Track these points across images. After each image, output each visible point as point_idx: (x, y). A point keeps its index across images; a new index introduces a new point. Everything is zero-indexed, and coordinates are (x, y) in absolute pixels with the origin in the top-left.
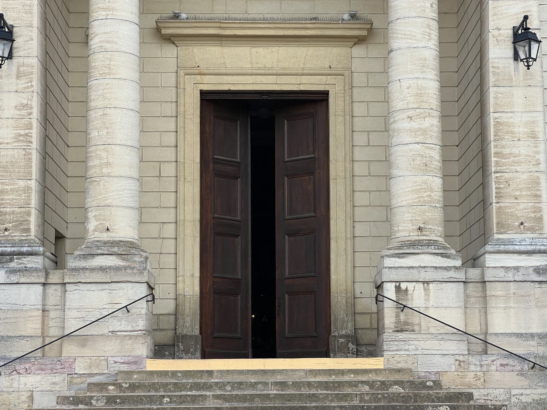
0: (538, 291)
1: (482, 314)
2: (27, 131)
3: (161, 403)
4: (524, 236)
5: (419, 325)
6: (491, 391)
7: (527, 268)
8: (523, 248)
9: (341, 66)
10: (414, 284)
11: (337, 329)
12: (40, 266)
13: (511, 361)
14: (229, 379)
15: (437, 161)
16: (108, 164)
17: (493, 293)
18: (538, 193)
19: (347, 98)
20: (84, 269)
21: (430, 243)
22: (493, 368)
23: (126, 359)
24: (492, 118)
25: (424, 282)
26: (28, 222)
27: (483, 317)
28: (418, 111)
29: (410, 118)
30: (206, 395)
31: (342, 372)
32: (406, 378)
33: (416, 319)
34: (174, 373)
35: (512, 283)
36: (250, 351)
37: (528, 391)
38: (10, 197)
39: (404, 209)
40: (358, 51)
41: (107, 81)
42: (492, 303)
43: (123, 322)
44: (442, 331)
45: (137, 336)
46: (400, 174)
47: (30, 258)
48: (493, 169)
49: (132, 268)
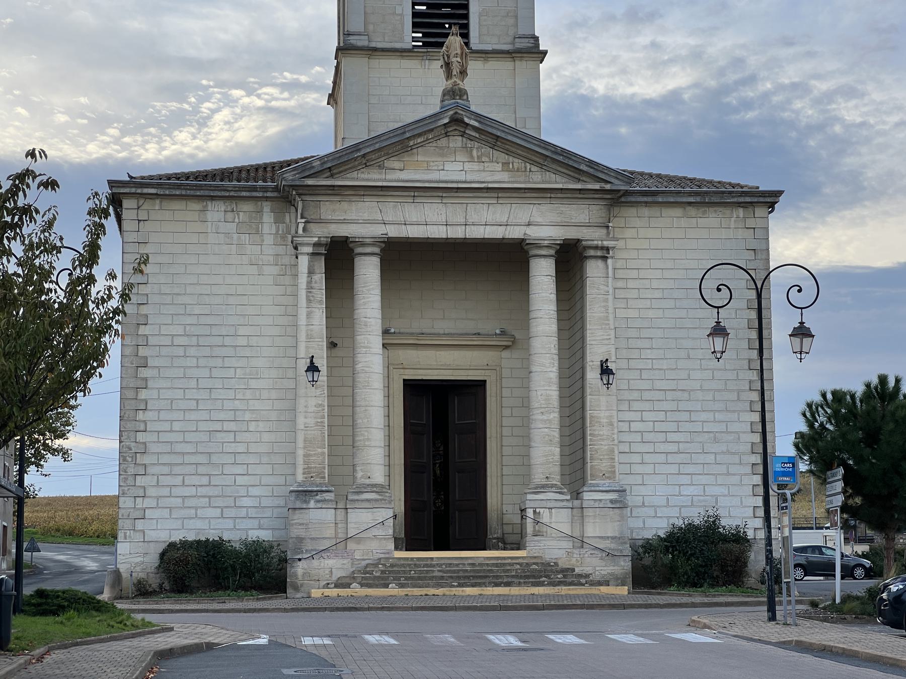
0: (612, 513)
1: (581, 526)
2: (322, 420)
3: (410, 574)
4: (605, 481)
5: (546, 532)
6: (584, 568)
7: (606, 500)
8: (604, 489)
9: (495, 364)
11: (491, 534)
12: (333, 498)
13: (596, 552)
14: (442, 562)
16: (368, 439)
17: (588, 514)
18: (613, 457)
19: (498, 385)
20: (357, 500)
21: (552, 486)
22: (586, 555)
23: (384, 551)
24: (588, 413)
25: (549, 508)
26: (324, 473)
27: (581, 528)
29: (542, 413)
30: (362, 585)
31: (504, 558)
32: (539, 561)
33: (545, 529)
34: (412, 559)
36: (432, 547)
37: (605, 568)
38: (314, 458)
39: (538, 466)
40: (505, 354)
41: (366, 390)
42: (586, 520)
43: (380, 530)
44: (558, 536)
45: (389, 538)
46: (536, 445)
47: (327, 494)
48: (589, 443)
49: (385, 500)
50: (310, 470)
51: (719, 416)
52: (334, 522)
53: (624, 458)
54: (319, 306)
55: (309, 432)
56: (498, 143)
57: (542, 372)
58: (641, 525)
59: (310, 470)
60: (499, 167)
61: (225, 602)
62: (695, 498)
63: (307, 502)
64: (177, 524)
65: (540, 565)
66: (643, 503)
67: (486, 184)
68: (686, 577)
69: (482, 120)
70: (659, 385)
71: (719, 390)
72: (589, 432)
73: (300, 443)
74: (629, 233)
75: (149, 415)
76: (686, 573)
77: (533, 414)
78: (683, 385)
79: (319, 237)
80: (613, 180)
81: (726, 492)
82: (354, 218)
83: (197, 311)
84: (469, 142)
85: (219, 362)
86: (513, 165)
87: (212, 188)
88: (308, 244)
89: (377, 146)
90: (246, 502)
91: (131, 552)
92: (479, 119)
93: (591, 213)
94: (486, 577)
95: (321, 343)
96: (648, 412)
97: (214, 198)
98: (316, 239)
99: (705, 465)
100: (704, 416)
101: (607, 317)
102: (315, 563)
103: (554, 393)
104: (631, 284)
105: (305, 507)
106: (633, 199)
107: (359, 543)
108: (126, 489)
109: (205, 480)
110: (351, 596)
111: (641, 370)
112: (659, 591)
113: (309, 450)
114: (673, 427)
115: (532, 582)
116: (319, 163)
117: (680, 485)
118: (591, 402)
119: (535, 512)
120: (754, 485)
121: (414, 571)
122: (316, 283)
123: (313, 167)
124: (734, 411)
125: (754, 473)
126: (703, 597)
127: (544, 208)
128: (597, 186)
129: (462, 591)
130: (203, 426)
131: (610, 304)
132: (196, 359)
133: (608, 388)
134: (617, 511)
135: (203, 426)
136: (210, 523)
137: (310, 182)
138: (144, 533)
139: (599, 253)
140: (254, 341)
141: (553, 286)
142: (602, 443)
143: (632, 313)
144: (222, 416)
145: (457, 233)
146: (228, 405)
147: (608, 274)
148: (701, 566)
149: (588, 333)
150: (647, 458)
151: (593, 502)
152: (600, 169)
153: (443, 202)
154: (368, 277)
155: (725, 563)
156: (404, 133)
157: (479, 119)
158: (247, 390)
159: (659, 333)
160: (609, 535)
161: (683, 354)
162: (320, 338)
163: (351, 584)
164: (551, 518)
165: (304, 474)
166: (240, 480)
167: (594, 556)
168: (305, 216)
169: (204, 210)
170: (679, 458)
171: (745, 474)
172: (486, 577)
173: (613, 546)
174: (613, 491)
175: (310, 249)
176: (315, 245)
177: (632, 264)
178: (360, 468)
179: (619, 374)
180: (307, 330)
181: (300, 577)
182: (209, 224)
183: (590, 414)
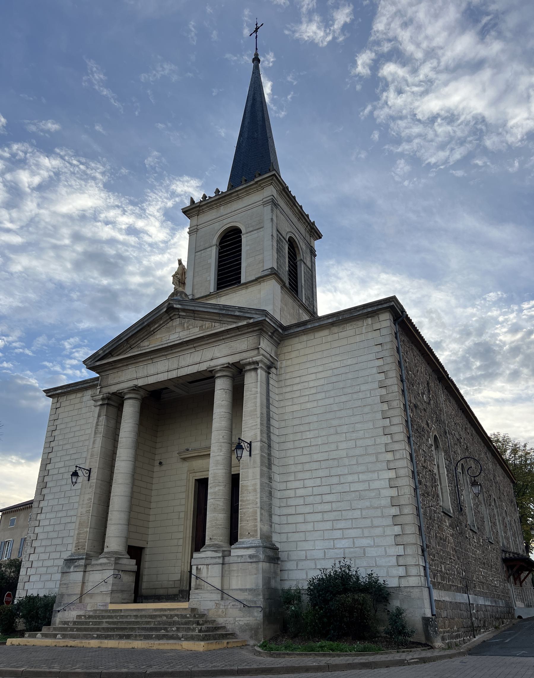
4: (250, 539)
5: (204, 586)
10: (203, 566)
15: (221, 506)
18: (256, 518)
22: (229, 607)
25: (207, 565)
28: (213, 484)
35: (240, 564)
37: (242, 619)
51: (362, 477)
55: (82, 518)
56: (196, 315)
60: (197, 329)
62: (347, 550)
65: (180, 616)
66: (306, 557)
69: (182, 303)
70: (316, 457)
74: (294, 354)
78: (334, 455)
80: (254, 316)
81: (372, 543)
87: (82, 383)
89: (130, 334)
92: (180, 303)
96: (309, 480)
100: (350, 478)
101: (256, 409)
107: (91, 598)
113: (80, 530)
114: (326, 489)
116: (102, 352)
117: (334, 540)
119: (197, 568)
123: (100, 355)
124: (374, 471)
128: (245, 323)
134: (254, 565)
139: (253, 367)
143: (296, 408)
145: (173, 375)
150: (309, 518)
151: (236, 557)
157: (180, 303)
159: (315, 418)
161: (332, 431)
164: (207, 573)
165: (75, 547)
167: (236, 607)
170: (332, 516)
171: (388, 526)
173: (250, 597)
174: (252, 547)
176: (103, 399)
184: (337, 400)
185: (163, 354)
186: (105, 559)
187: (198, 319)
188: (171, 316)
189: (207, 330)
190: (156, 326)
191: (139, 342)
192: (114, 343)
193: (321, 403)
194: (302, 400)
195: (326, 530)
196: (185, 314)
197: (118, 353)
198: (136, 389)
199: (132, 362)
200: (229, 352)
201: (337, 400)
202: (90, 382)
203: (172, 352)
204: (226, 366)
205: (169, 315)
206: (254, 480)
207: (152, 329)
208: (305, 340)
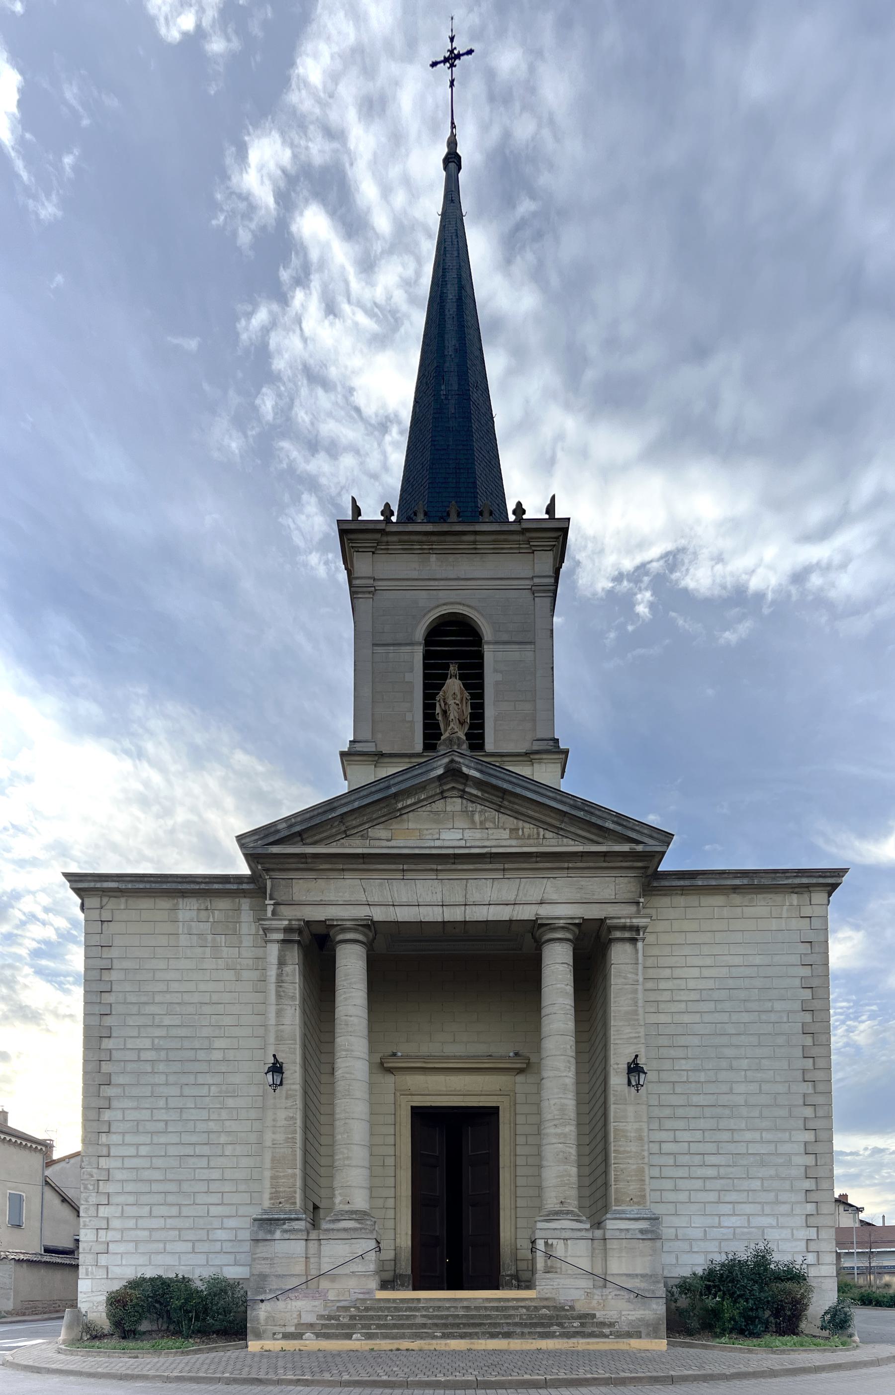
3: (386, 1320)
4: (633, 1208)
5: (561, 1268)
6: (607, 1312)
7: (634, 1230)
8: (632, 1216)
13: (622, 1293)
14: (432, 1304)
16: (348, 1158)
17: (611, 1247)
20: (333, 1230)
21: (568, 1212)
22: (610, 1297)
23: (362, 1291)
24: (612, 1126)
25: (564, 1239)
26: (295, 1198)
30: (318, 1335)
31: (508, 1300)
33: (558, 1264)
34: (394, 1300)
36: (445, 1285)
40: (520, 1078)
45: (369, 1275)
47: (297, 1222)
48: (613, 1162)
49: (365, 1229)
50: (278, 1195)
51: (767, 1136)
52: (304, 1255)
53: (656, 1184)
54: (291, 1003)
55: (277, 1150)
57: (556, 1077)
58: (674, 1261)
59: (278, 1195)
60: (506, 834)
61: (137, 1357)
62: (738, 1231)
63: (272, 1232)
64: (142, 1260)
66: (676, 1235)
67: (489, 849)
68: (732, 1322)
69: (484, 769)
70: (695, 1099)
71: (767, 1106)
72: (612, 1148)
73: (268, 1164)
75: (115, 1138)
76: (732, 1319)
77: (545, 1128)
78: (723, 1100)
79: (290, 920)
80: (646, 840)
81: (774, 1223)
82: (332, 898)
83: (167, 1022)
84: (470, 804)
85: (191, 1079)
86: (523, 831)
87: (179, 880)
88: (277, 930)
89: (356, 805)
90: (221, 1235)
91: (94, 1290)
92: (480, 767)
93: (617, 887)
94: (480, 1325)
95: (292, 1046)
97: (185, 895)
98: (286, 922)
99: (750, 1193)
100: (748, 1136)
101: (637, 1011)
102: (281, 1305)
103: (570, 1102)
104: (663, 985)
105: (269, 1238)
106: (667, 883)
108: (87, 1220)
109: (174, 1211)
110: (300, 1350)
111: (674, 1083)
112: (704, 1342)
113: (277, 1171)
114: (712, 1148)
115: (539, 1332)
116: (284, 825)
117: (719, 1216)
118: (615, 1112)
119: (546, 1243)
120: (807, 1215)
121: (391, 1316)
122: (287, 975)
123: (278, 831)
124: (785, 1130)
125: (808, 1200)
126: (767, 1354)
127: (560, 882)
128: (626, 848)
129: (446, 1344)
130: (172, 1150)
131: (640, 995)
132: (165, 1076)
133: (638, 1090)
134: (648, 1243)
135: (172, 1150)
136: (179, 1258)
137: (275, 849)
138: (107, 1268)
139: (627, 935)
140: (231, 1055)
141: (570, 977)
142: (630, 1161)
143: (663, 1018)
144: (194, 1139)
145: (455, 915)
146: (201, 1126)
147: (637, 959)
148: (752, 1309)
149: (613, 1032)
150: (682, 1184)
152: (630, 825)
153: (439, 877)
154: (349, 969)
155: (782, 1306)
156: (388, 787)
157: (480, 767)
158: (222, 1110)
159: (696, 1041)
160: (639, 1271)
161: (724, 1064)
162: (292, 1040)
163: (303, 1334)
164: (566, 1251)
165: (271, 1199)
166: (214, 1210)
168: (275, 896)
169: (175, 909)
170: (718, 1185)
171: (798, 1202)
172: (480, 1325)
173: (643, 1285)
174: (644, 1219)
175: (280, 936)
176: (288, 930)
177: (663, 962)
178: (339, 1191)
179: (652, 1076)
180: (277, 1031)
181: (262, 1321)
182: (181, 924)
183: (614, 1126)
184: (735, 1017)
185: (434, 867)
186: (353, 1222)
187: (509, 812)
188: (445, 787)
189: (527, 841)
190: (409, 802)
191: (367, 826)
192: (315, 813)
193: (707, 1018)
194: (674, 1007)
195: (708, 1202)
196: (479, 794)
197: (316, 838)
198: (370, 926)
199: (355, 866)
200: (577, 897)
201: (735, 1017)
202: (202, 882)
203: (454, 867)
204: (577, 921)
205: (441, 785)
206: (638, 1124)
207: (400, 805)
208: (682, 904)
